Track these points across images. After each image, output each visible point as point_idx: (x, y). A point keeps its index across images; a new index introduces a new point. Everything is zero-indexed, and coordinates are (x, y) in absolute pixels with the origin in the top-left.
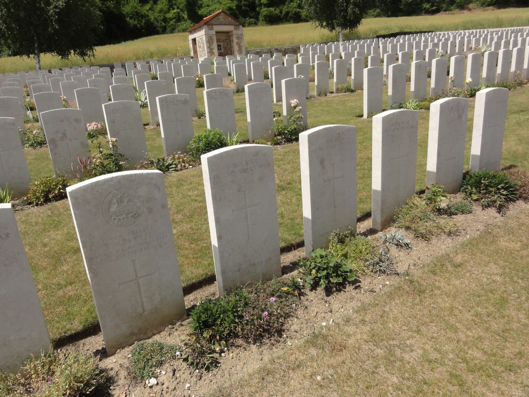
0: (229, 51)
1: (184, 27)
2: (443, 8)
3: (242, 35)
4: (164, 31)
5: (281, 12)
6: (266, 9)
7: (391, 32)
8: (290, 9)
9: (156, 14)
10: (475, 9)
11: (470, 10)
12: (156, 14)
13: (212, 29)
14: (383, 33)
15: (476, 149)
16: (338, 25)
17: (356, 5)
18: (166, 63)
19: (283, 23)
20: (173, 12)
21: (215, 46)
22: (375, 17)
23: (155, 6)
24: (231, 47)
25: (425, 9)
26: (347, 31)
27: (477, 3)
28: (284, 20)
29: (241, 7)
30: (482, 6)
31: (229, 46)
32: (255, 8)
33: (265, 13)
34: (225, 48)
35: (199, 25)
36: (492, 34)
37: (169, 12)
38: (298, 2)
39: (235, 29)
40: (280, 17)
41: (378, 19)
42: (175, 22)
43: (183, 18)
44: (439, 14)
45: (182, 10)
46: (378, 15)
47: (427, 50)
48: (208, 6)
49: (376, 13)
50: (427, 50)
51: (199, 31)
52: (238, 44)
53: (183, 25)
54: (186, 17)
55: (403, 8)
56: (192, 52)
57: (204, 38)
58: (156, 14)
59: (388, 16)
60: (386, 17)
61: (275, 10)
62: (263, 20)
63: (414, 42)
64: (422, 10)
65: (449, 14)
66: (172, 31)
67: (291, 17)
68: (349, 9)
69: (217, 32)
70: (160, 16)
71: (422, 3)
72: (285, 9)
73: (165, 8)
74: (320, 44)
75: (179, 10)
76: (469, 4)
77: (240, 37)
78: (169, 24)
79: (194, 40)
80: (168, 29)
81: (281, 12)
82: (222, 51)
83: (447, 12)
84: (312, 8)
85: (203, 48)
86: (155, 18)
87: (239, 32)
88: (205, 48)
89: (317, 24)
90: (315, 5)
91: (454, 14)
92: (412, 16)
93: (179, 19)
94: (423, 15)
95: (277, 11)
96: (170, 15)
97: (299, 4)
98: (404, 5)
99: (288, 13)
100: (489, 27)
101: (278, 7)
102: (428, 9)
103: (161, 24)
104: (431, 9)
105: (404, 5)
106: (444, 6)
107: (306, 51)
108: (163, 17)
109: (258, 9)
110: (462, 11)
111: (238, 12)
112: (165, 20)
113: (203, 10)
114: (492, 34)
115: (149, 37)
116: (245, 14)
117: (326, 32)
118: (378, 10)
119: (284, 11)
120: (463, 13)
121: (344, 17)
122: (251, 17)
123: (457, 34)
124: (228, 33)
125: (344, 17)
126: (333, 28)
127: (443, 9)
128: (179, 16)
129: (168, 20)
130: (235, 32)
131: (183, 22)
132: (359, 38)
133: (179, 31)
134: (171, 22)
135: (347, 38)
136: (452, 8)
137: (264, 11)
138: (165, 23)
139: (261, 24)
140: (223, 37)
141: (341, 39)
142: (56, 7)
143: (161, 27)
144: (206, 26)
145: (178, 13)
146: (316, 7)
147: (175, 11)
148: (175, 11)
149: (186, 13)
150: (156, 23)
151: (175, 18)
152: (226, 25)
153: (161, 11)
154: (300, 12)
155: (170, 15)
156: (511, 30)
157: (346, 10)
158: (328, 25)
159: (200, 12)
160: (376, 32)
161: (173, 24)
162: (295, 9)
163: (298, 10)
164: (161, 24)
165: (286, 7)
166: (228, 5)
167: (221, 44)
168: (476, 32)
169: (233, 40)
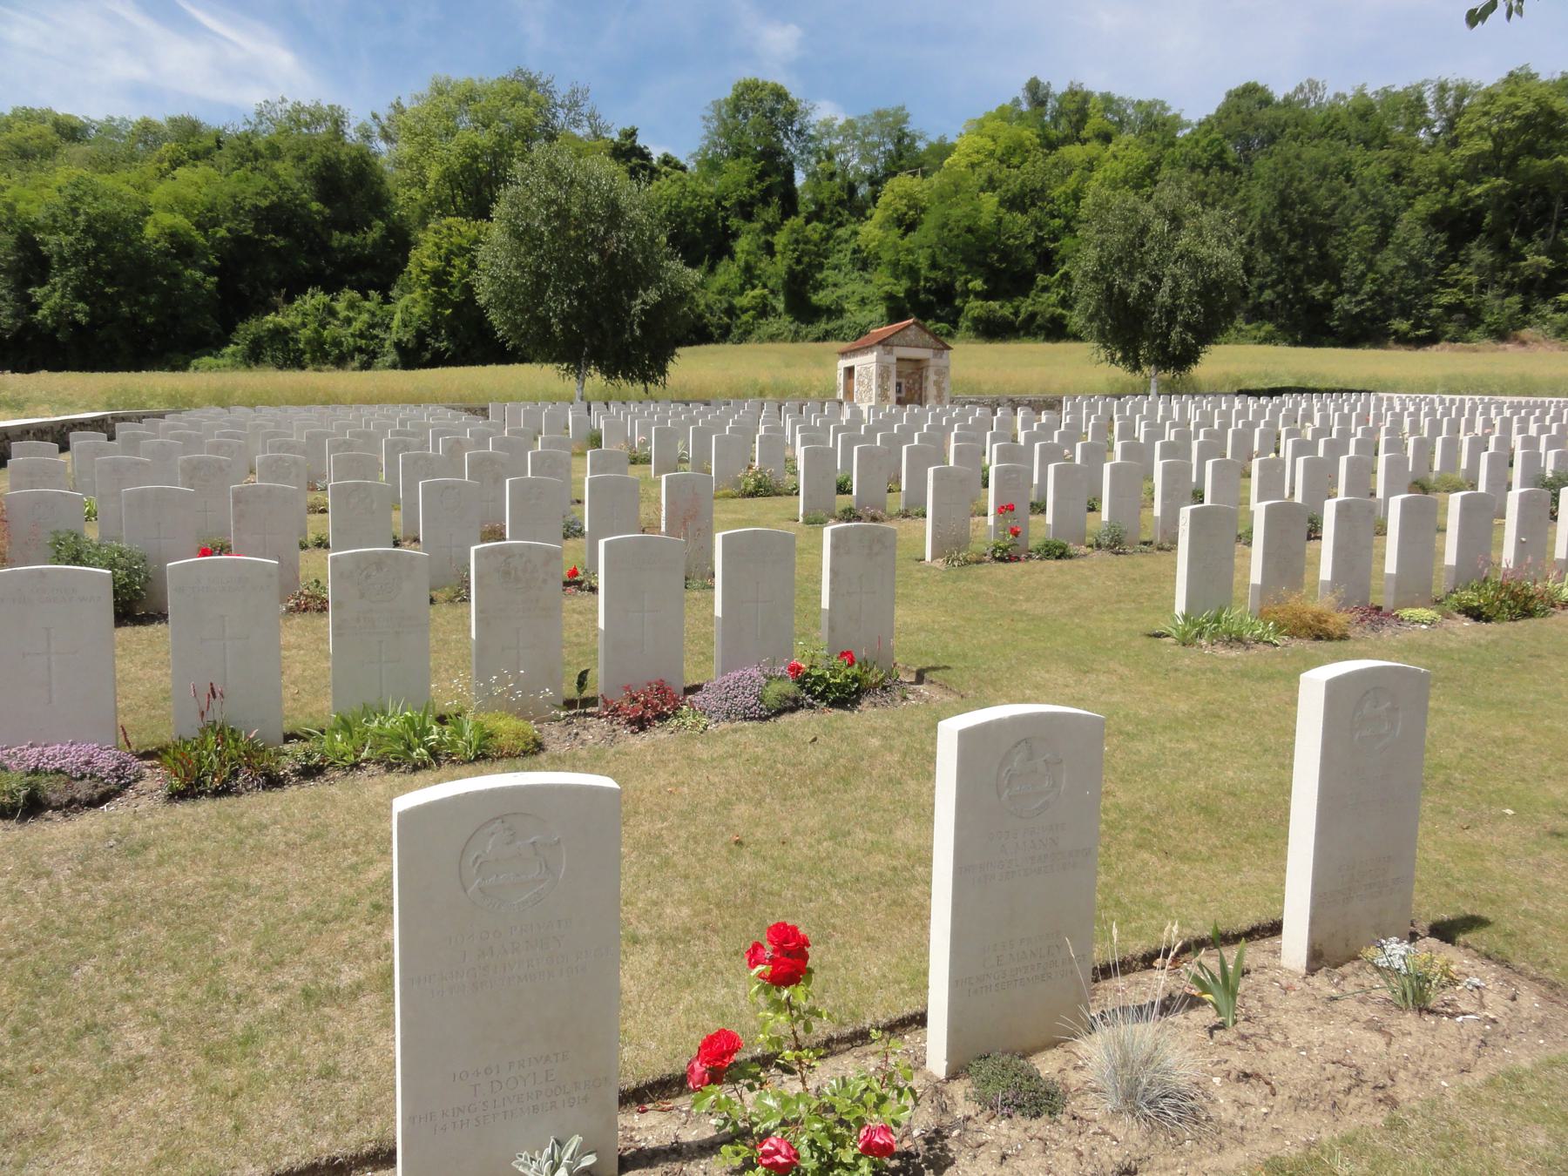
0: (916, 396)
1: (773, 329)
2: (1447, 333)
3: (947, 367)
4: (724, 335)
5: (1016, 313)
6: (980, 303)
7: (1273, 385)
8: (1038, 308)
9: (710, 295)
10: (1536, 341)
11: (1524, 343)
12: (710, 295)
13: (890, 353)
14: (1254, 384)
15: (1194, 480)
16: (1149, 362)
17: (1187, 326)
18: (613, 409)
19: (1018, 337)
20: (752, 293)
21: (893, 381)
22: (1260, 343)
23: (710, 279)
24: (921, 388)
25: (1396, 332)
26: (1167, 375)
27: (1545, 327)
28: (1022, 333)
29: (917, 293)
30: (1558, 335)
31: (917, 386)
32: (953, 298)
33: (976, 313)
34: (909, 390)
35: (804, 330)
36: (1486, 411)
37: (741, 294)
38: (1062, 292)
39: (935, 356)
40: (1012, 323)
41: (1268, 349)
42: (754, 318)
43: (774, 309)
44: (1435, 347)
45: (772, 292)
46: (1267, 339)
47: (1439, 441)
48: (835, 285)
49: (1262, 334)
50: (1439, 441)
51: (863, 354)
52: (938, 384)
53: (772, 325)
54: (781, 307)
55: (1337, 326)
56: (842, 391)
57: (873, 368)
58: (711, 297)
59: (1296, 344)
60: (1290, 345)
61: (1001, 307)
62: (968, 329)
63: (1445, 419)
64: (1388, 336)
65: (1462, 349)
66: (744, 337)
67: (1040, 327)
68: (1173, 334)
69: (899, 359)
70: (720, 302)
71: (1389, 318)
72: (1026, 306)
73: (735, 285)
74: (1106, 396)
75: (766, 291)
76: (1522, 327)
77: (942, 372)
78: (739, 322)
79: (850, 371)
80: (736, 332)
81: (1016, 313)
82: (903, 394)
83: (1459, 344)
84: (1095, 324)
85: (869, 385)
86: (707, 306)
87: (941, 362)
88: (873, 387)
89: (1103, 357)
90: (1101, 320)
91: (1476, 351)
92: (1363, 347)
93: (763, 311)
94: (1390, 348)
95: (1007, 311)
96: (741, 301)
97: (1064, 297)
98: (1338, 319)
99: (1033, 316)
100: (1504, 392)
101: (1010, 299)
102: (1406, 334)
103: (720, 318)
104: (1412, 335)
105: (1340, 319)
106: (1451, 328)
107: (1076, 409)
108: (725, 305)
109: (958, 302)
110: (1502, 346)
111: (908, 306)
112: (731, 311)
113: (821, 294)
114: (1486, 411)
115: (695, 348)
116: (924, 312)
117: (1121, 373)
118: (1269, 327)
119: (1023, 310)
120: (1505, 349)
121: (1163, 348)
122: (939, 319)
123: (1421, 400)
124: (918, 361)
125: (1163, 348)
126: (1136, 367)
127: (1448, 336)
128: (765, 305)
129: (738, 312)
130: (933, 362)
131: (771, 319)
132: (1194, 391)
133: (760, 340)
134: (745, 318)
135: (1169, 390)
136: (1472, 334)
137: (975, 307)
138: (731, 319)
139: (963, 338)
140: (908, 368)
141: (1153, 391)
142: (644, 303)
143: (720, 327)
144: (880, 347)
145: (764, 297)
146: (1104, 325)
147: (757, 292)
148: (757, 292)
149: (782, 298)
150: (708, 315)
151: (754, 308)
152: (917, 347)
153: (722, 291)
154: (1064, 317)
155: (741, 301)
156: (1512, 403)
157: (1166, 335)
158: (1124, 359)
159: (814, 299)
160: (1239, 381)
161: (747, 322)
162: (1051, 309)
163: (1059, 311)
164: (720, 318)
165: (1029, 301)
166: (887, 288)
167: (903, 381)
168: (1462, 402)
169: (927, 377)
